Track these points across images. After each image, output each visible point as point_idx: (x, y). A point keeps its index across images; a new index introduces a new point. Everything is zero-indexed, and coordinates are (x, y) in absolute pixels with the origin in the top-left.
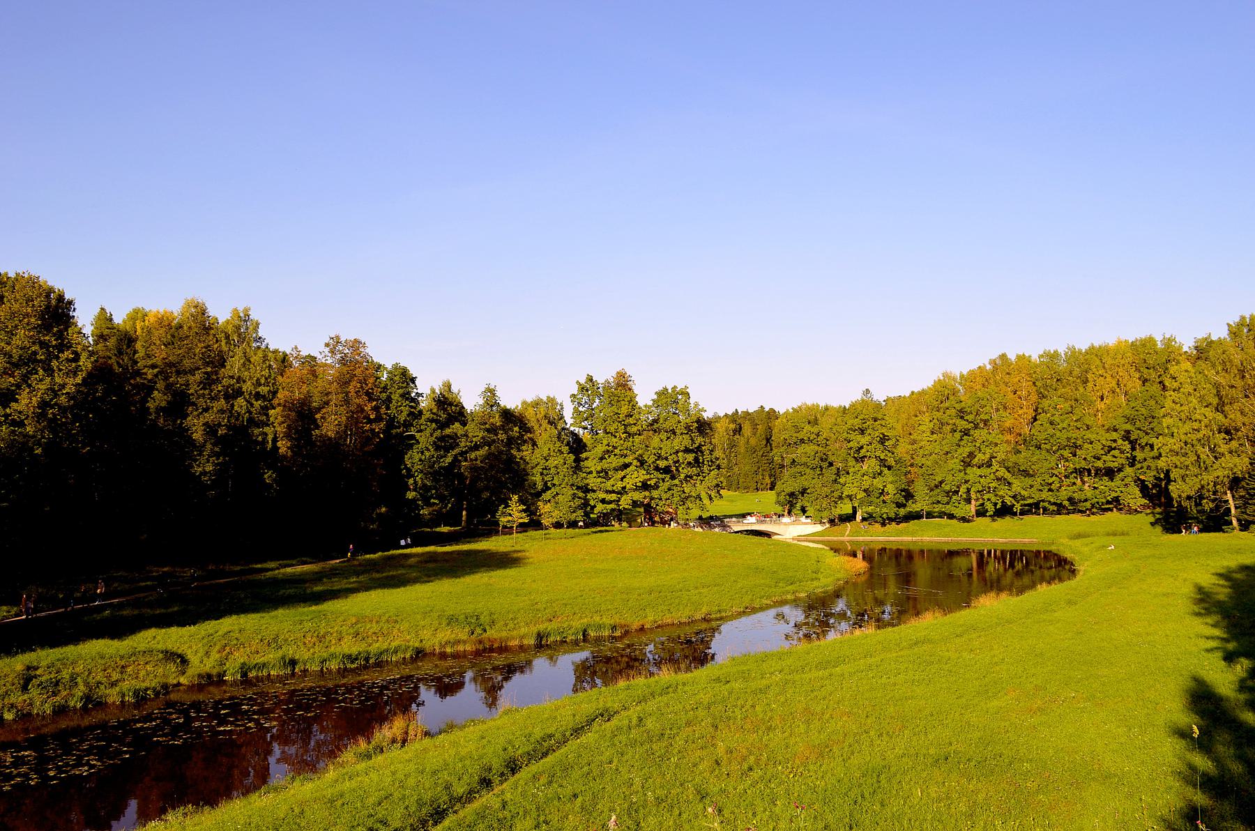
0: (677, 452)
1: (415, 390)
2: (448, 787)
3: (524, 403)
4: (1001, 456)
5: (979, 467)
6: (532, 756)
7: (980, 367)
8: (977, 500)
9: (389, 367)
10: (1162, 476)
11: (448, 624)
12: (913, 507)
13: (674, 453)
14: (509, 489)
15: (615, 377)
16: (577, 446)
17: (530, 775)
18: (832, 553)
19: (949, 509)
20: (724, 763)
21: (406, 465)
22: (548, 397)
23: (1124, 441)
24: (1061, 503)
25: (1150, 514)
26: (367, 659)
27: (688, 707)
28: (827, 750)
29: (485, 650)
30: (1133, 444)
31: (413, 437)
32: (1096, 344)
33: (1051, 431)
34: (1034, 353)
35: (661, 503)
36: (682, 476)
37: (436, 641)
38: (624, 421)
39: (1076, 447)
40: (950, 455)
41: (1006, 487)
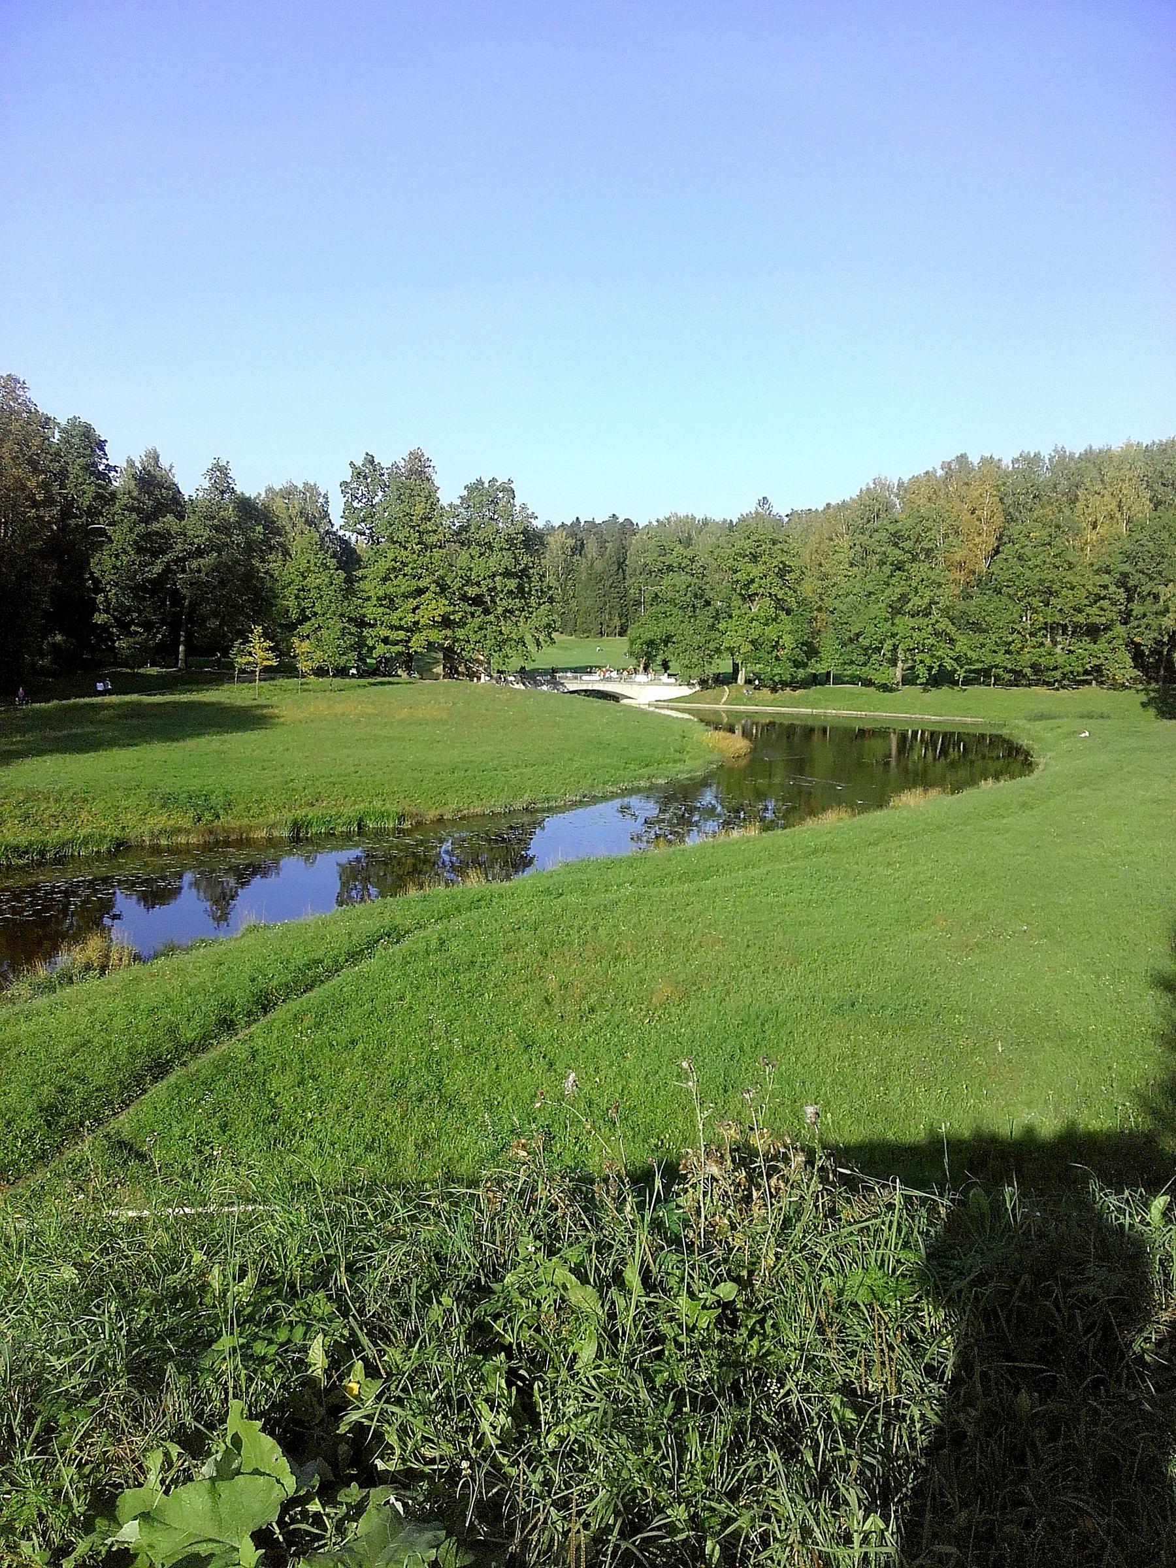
0: (494, 576)
1: (104, 461)
2: (172, 1030)
3: (270, 490)
4: (943, 602)
5: (913, 616)
6: (291, 989)
7: (927, 473)
8: (904, 662)
9: (63, 422)
10: (1166, 639)
11: (163, 806)
12: (817, 668)
13: (489, 577)
14: (248, 616)
15: (407, 459)
16: (348, 558)
17: (289, 1015)
18: (702, 726)
19: (866, 672)
20: (556, 1002)
21: (92, 573)
22: (306, 484)
23: (1118, 587)
24: (1021, 671)
25: (1142, 690)
26: (42, 854)
27: (507, 927)
28: (694, 988)
29: (217, 844)
30: (1131, 593)
31: (102, 532)
32: (1095, 447)
33: (1018, 569)
34: (1006, 456)
35: (468, 647)
36: (500, 610)
37: (145, 829)
38: (419, 526)
39: (1051, 594)
40: (873, 597)
41: (948, 645)
